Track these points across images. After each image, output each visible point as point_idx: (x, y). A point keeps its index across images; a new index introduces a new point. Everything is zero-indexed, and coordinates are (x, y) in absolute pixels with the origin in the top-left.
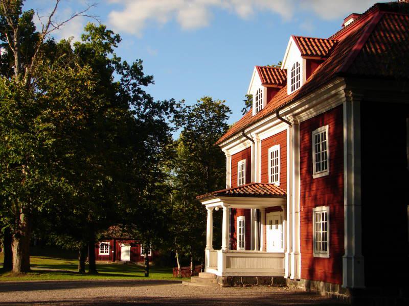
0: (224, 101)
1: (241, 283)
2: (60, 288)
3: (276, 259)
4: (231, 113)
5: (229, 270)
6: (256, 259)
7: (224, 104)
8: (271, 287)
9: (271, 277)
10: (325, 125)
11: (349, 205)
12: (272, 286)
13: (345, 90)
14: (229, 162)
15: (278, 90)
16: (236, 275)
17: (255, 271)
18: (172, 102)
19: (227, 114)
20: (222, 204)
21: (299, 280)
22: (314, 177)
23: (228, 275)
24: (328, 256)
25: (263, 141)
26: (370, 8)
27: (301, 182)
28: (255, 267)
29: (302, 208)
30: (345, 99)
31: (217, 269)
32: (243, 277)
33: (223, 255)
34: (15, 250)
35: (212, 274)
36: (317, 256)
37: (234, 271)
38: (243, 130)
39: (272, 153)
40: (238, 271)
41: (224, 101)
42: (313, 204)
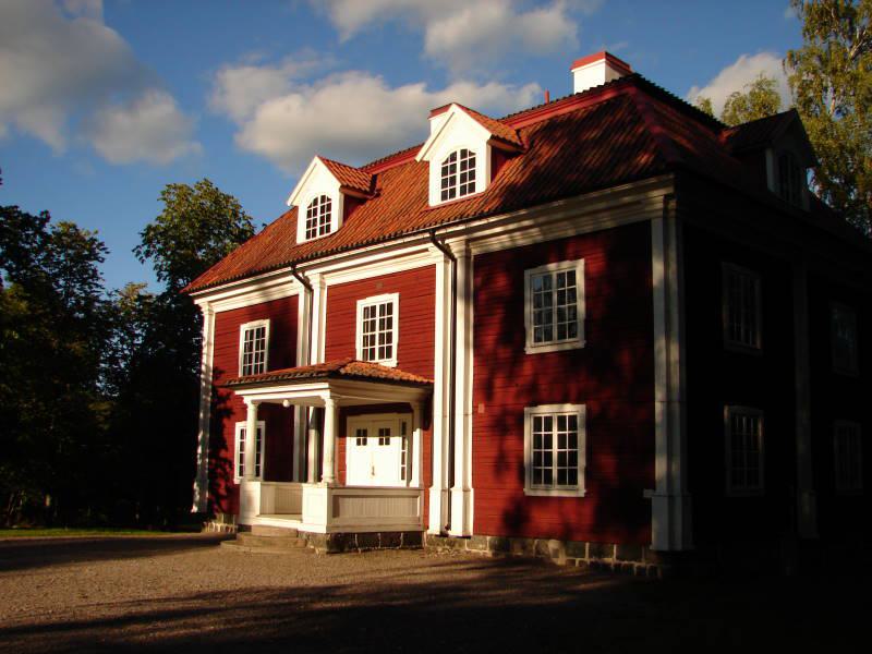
0: (96, 232)
1: (355, 546)
2: (46, 563)
3: (407, 499)
4: (107, 253)
5: (337, 521)
6: (378, 499)
7: (95, 237)
8: (402, 552)
9: (400, 533)
10: (577, 257)
11: (668, 402)
12: (402, 548)
13: (667, 198)
14: (210, 325)
15: (362, 201)
16: (348, 530)
17: (375, 523)
18: (44, 217)
19: (102, 254)
20: (326, 395)
21: (469, 537)
22: (531, 349)
23: (336, 531)
24: (582, 492)
25: (330, 288)
26: (591, 88)
27: (475, 361)
28: (377, 515)
29: (481, 408)
30: (661, 213)
31: (301, 520)
32: (358, 534)
33: (329, 494)
34: (760, 426)
35: (289, 529)
36: (532, 494)
37: (346, 524)
38: (293, 265)
39: (370, 311)
40: (352, 523)
41: (96, 232)
42: (524, 401)
